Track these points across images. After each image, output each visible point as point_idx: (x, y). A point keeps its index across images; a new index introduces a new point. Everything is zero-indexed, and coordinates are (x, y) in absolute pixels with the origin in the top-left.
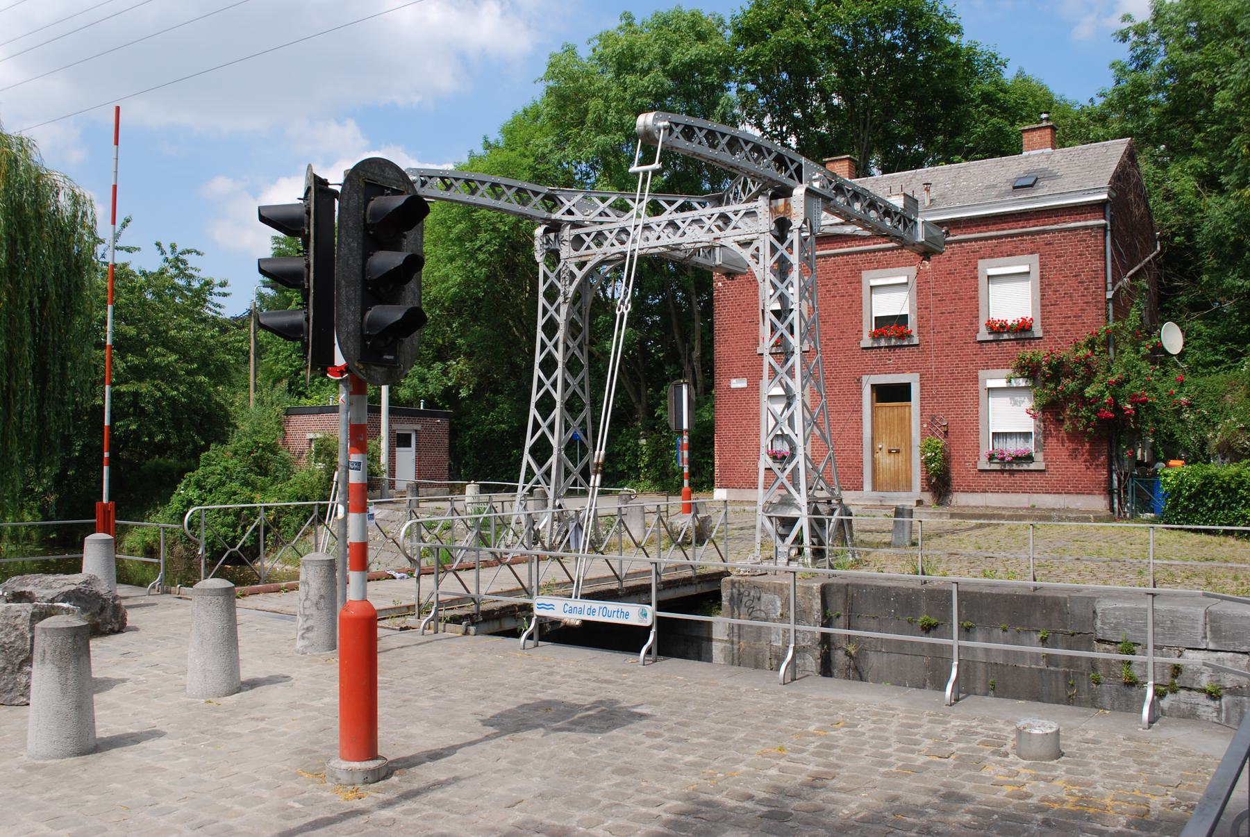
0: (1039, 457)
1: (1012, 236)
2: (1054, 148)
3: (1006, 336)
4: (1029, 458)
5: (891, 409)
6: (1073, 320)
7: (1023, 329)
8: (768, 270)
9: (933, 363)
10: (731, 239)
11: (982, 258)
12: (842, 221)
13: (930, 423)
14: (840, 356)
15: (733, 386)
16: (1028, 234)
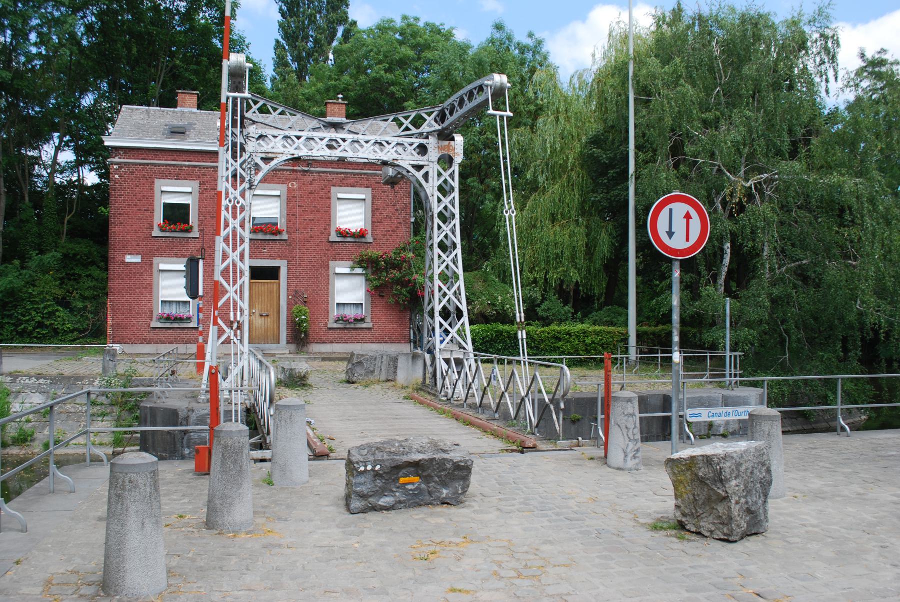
0: (368, 319)
1: (354, 174)
2: (199, 107)
3: (349, 239)
4: (362, 320)
5: (264, 284)
7: (362, 234)
8: (436, 189)
9: (297, 254)
10: (407, 162)
11: (334, 186)
13: (295, 297)
16: (365, 174)
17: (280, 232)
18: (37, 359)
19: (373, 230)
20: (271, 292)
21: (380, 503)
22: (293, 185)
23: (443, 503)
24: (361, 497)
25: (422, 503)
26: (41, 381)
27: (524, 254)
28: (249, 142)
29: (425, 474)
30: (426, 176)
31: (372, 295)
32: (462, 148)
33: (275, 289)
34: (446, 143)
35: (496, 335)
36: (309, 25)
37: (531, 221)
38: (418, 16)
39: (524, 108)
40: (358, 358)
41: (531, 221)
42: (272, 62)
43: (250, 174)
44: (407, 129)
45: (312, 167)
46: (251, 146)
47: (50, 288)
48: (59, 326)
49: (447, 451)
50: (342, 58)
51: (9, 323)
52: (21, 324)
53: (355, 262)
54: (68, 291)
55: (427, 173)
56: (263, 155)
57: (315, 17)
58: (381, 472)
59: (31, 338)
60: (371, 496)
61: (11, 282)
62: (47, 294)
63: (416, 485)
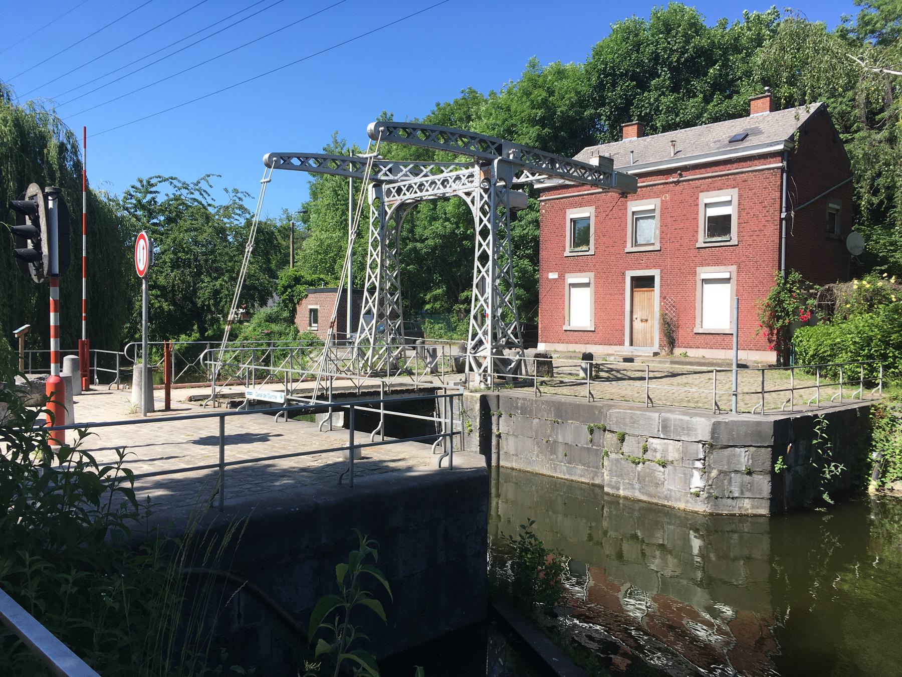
6: (758, 233)
8: (479, 210)
10: (461, 191)
11: (701, 192)
12: (547, 176)
14: (613, 258)
22: (666, 196)
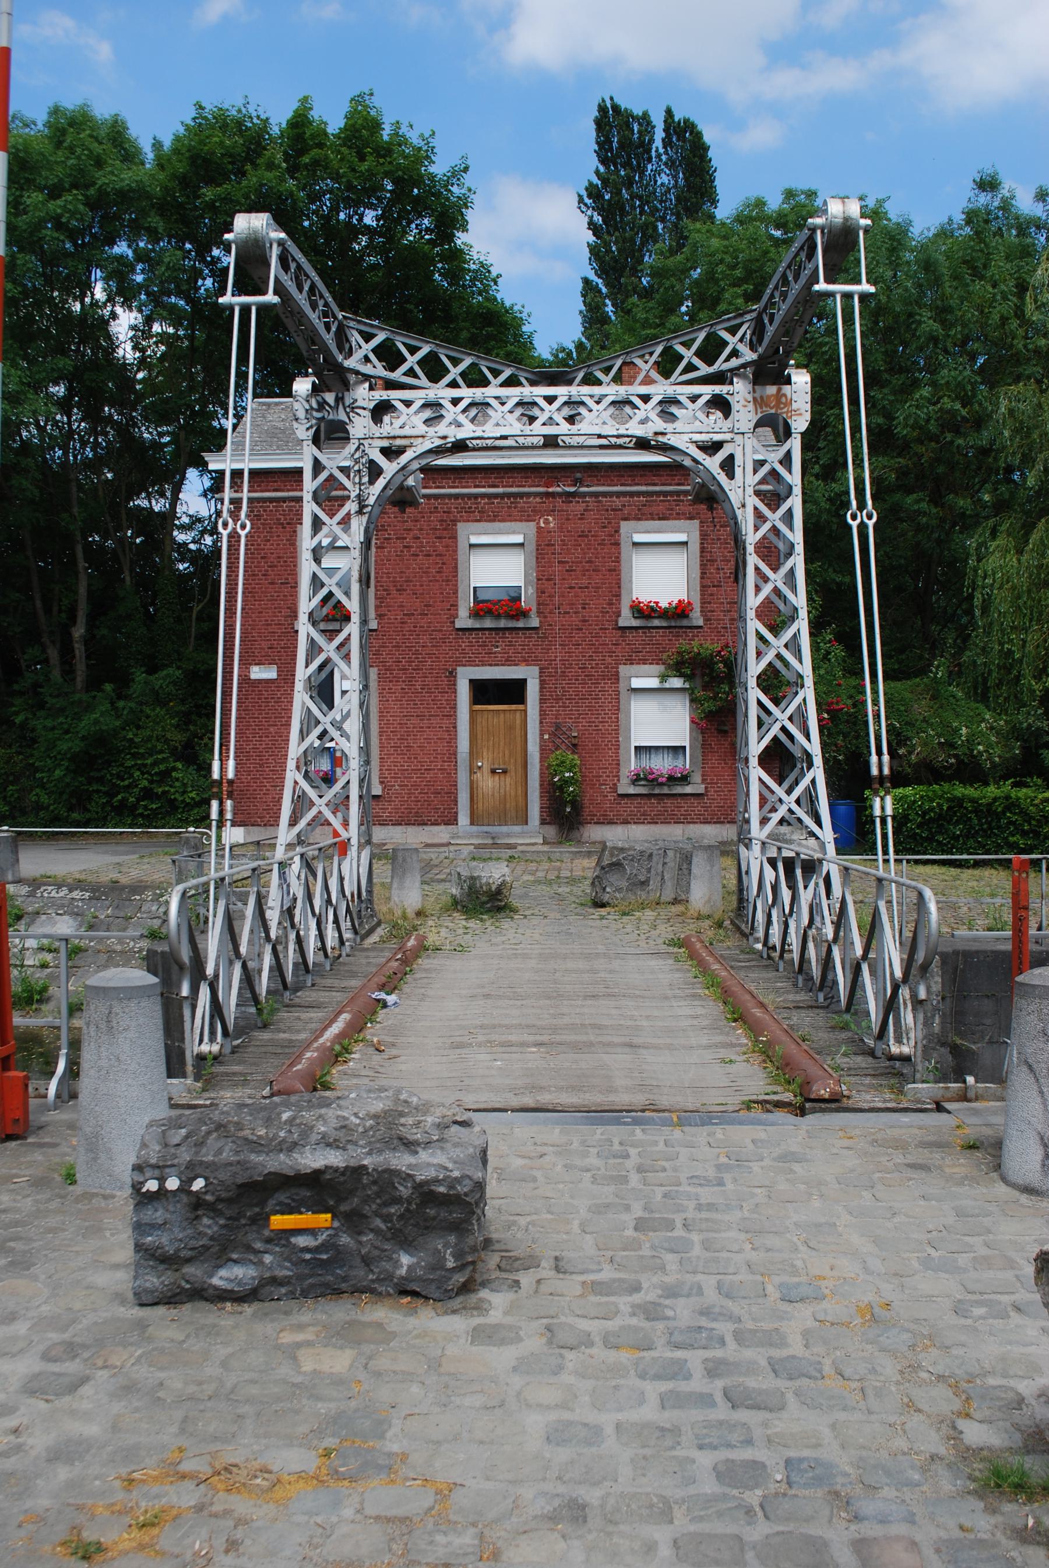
0: (697, 778)
1: (665, 494)
3: (656, 623)
4: (684, 779)
7: (680, 611)
8: (750, 491)
9: (557, 653)
10: (686, 437)
11: (626, 519)
15: (253, 676)
17: (525, 614)
18: (106, 852)
19: (703, 602)
20: (511, 728)
21: (215, 1281)
22: (547, 522)
23: (404, 1292)
24: (162, 1262)
25: (344, 1286)
26: (77, 894)
27: (1024, 641)
28: (356, 419)
29: (344, 1207)
30: (728, 465)
31: (703, 731)
32: (808, 398)
33: (518, 722)
34: (771, 390)
35: (949, 808)
36: (643, 244)
37: (1039, 574)
38: (813, 188)
39: (1025, 346)
40: (612, 855)
41: (1039, 574)
42: (580, 319)
43: (360, 484)
44: (690, 368)
45: (582, 485)
46: (360, 426)
47: (164, 730)
48: (177, 796)
49: (417, 1143)
50: (667, 284)
51: (98, 791)
52: (118, 793)
53: (669, 667)
54: (195, 735)
55: (731, 458)
56: (385, 443)
57: (656, 228)
58: (209, 1198)
59: (135, 817)
60: (188, 1260)
61: (96, 722)
62: (158, 740)
63: (322, 1238)
